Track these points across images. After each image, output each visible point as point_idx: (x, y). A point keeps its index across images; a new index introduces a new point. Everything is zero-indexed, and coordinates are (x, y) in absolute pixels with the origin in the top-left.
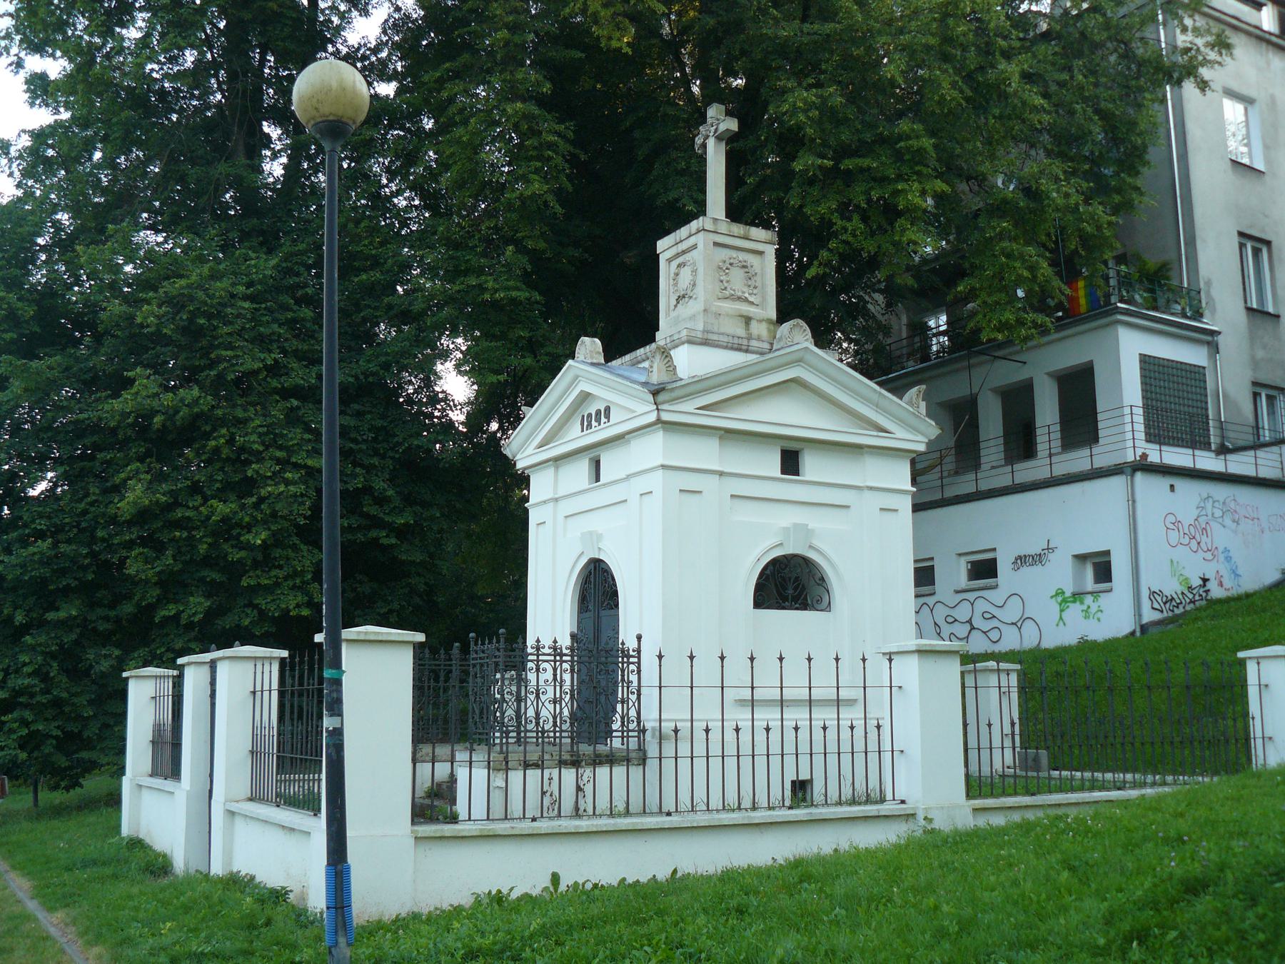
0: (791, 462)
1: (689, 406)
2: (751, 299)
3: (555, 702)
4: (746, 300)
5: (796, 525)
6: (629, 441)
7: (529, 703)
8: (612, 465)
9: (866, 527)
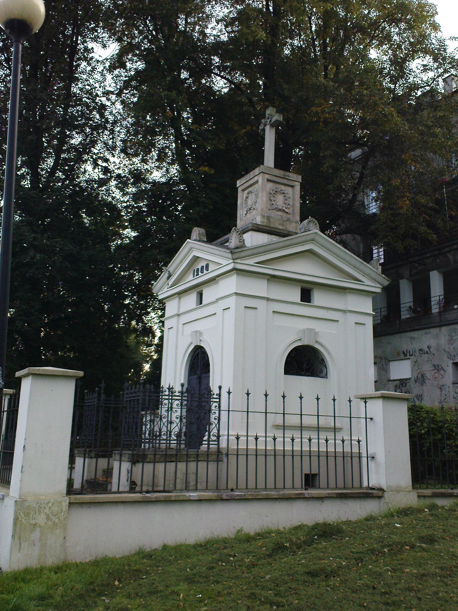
0: (306, 296)
1: (252, 261)
2: (287, 210)
3: (171, 423)
4: (284, 211)
5: (308, 329)
6: (218, 282)
7: (156, 423)
8: (209, 294)
9: (347, 334)
